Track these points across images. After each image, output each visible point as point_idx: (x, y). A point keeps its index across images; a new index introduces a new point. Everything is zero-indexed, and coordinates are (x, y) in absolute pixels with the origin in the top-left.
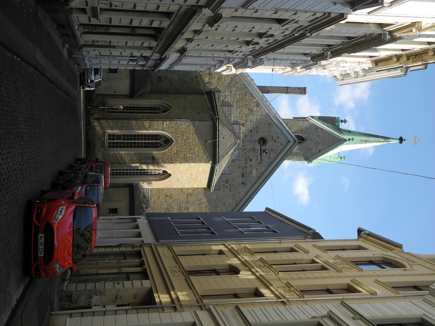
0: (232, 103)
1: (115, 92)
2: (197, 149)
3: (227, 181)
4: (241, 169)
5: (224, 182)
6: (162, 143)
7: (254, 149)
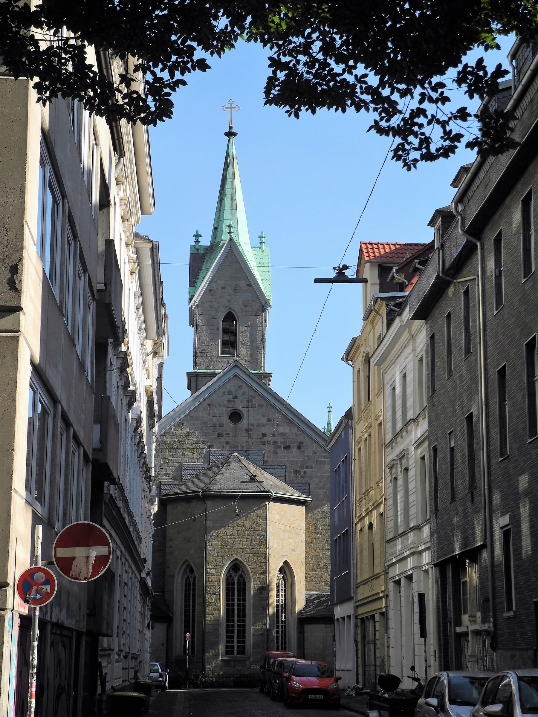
0: (178, 465)
1: (163, 644)
2: (247, 524)
3: (296, 472)
4: (278, 451)
5: (297, 477)
6: (238, 574)
7: (247, 430)
